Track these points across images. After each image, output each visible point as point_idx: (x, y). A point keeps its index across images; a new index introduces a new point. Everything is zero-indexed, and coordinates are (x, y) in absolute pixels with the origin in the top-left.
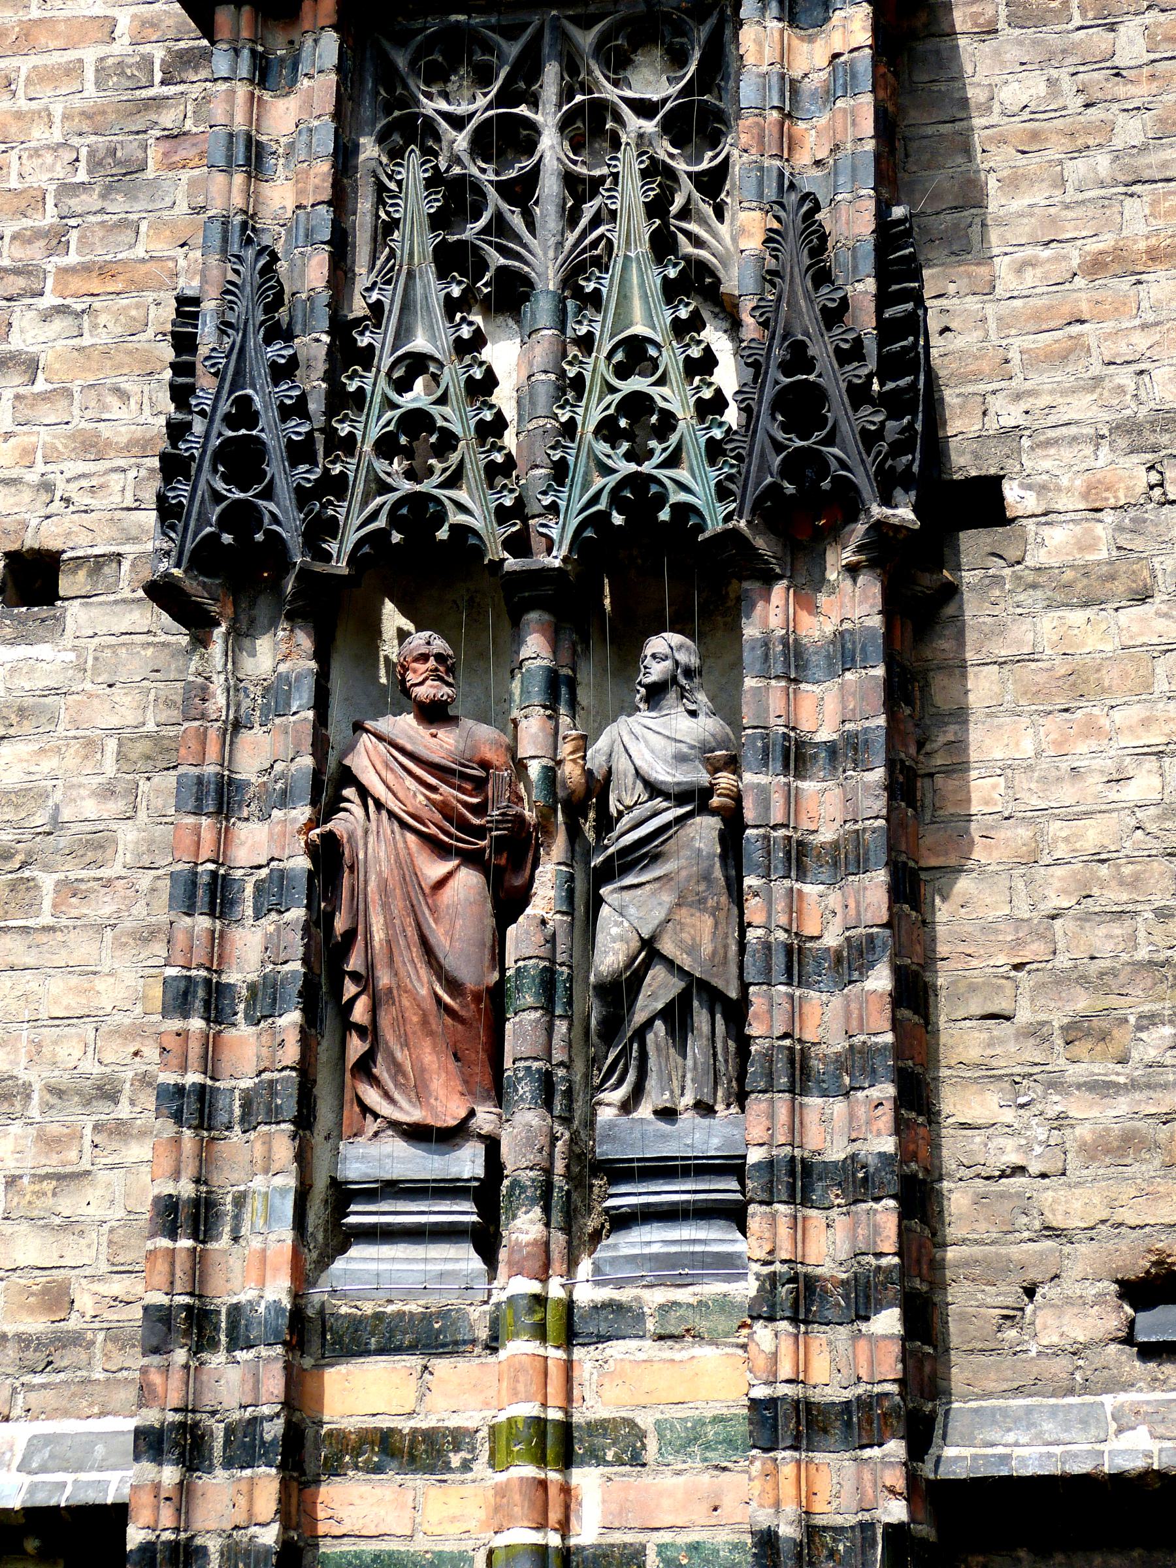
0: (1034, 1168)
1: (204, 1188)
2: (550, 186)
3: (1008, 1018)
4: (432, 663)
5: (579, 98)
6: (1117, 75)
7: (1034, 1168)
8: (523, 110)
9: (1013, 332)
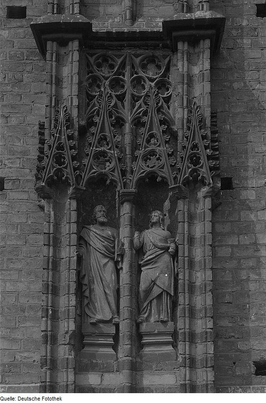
0: (236, 336)
1: (53, 333)
2: (128, 97)
3: (231, 303)
4: (102, 213)
5: (135, 75)
6: (260, 83)
7: (236, 336)
8: (121, 77)
9: (235, 143)
